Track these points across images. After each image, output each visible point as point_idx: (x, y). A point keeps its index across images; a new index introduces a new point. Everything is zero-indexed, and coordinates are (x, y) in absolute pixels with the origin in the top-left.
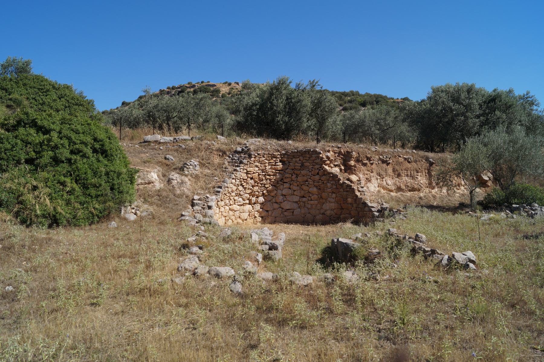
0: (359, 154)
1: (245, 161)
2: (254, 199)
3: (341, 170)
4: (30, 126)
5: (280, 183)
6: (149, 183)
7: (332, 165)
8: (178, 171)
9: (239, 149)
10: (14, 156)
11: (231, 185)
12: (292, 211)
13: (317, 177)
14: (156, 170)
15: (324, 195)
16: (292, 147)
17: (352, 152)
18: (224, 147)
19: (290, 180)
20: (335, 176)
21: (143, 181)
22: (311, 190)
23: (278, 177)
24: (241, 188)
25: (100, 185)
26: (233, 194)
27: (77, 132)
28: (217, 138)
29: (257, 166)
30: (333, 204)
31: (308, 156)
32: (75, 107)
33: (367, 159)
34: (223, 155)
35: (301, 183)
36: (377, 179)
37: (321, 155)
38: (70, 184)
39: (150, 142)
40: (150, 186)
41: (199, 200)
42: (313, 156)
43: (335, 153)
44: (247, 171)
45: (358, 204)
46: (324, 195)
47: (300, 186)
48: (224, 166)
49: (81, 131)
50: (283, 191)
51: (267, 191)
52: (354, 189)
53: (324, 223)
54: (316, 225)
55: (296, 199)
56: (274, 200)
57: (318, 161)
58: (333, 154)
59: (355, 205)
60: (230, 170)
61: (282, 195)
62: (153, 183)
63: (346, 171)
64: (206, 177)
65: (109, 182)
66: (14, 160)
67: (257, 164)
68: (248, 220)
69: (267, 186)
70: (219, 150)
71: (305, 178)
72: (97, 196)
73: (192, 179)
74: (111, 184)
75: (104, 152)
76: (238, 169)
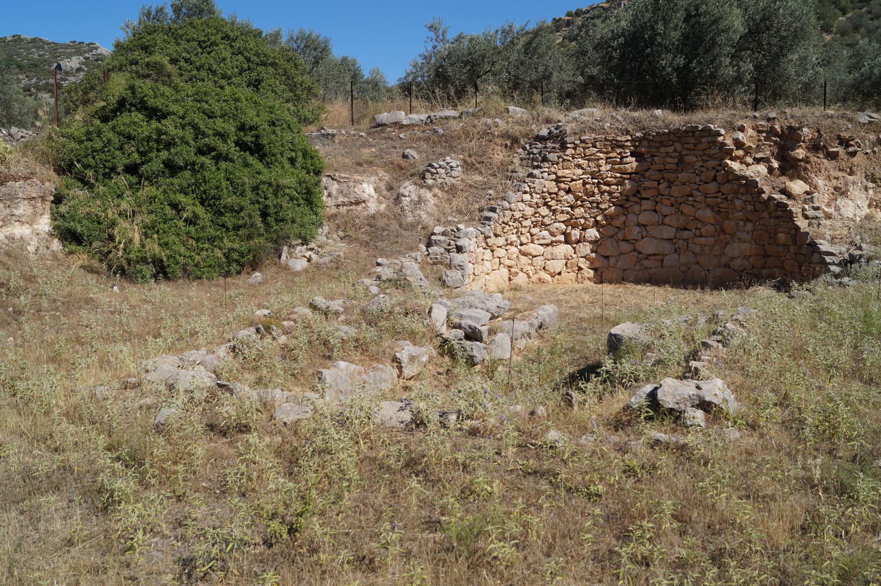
0: (818, 131)
1: (552, 156)
2: (576, 233)
3: (771, 170)
4: (137, 110)
5: (633, 199)
6: (358, 203)
7: (749, 160)
8: (416, 178)
9: (544, 132)
10: (106, 161)
11: (521, 206)
12: (659, 258)
13: (712, 187)
14: (373, 179)
15: (729, 225)
16: (660, 123)
17: (800, 128)
18: (516, 130)
19: (655, 192)
20: (751, 185)
21: (346, 200)
22: (699, 214)
23: (628, 187)
24: (544, 211)
25: (242, 209)
26: (528, 223)
27: (211, 116)
28: (508, 111)
29: (579, 166)
30: (747, 246)
31: (692, 141)
32: (260, 68)
33: (841, 144)
34: (512, 144)
35: (680, 200)
36: (866, 189)
37: (720, 139)
38: (191, 206)
39: (385, 125)
40: (360, 208)
41: (444, 234)
42: (703, 140)
43: (759, 132)
44: (558, 177)
45: (800, 247)
46: (729, 225)
47: (677, 205)
48: (510, 168)
49: (219, 113)
50: (641, 217)
51: (605, 216)
52: (791, 212)
53: (719, 284)
54: (702, 289)
55: (669, 232)
56: (620, 235)
57: (714, 151)
58: (755, 134)
59: (792, 249)
60: (521, 175)
61: (639, 225)
62: (364, 202)
63: (783, 171)
64: (473, 190)
65: (258, 202)
66: (105, 167)
67: (581, 161)
68: (563, 274)
69: (603, 206)
70: (505, 135)
71: (687, 189)
72: (237, 228)
73: (440, 194)
74: (261, 206)
75: (257, 150)
76: (536, 172)
